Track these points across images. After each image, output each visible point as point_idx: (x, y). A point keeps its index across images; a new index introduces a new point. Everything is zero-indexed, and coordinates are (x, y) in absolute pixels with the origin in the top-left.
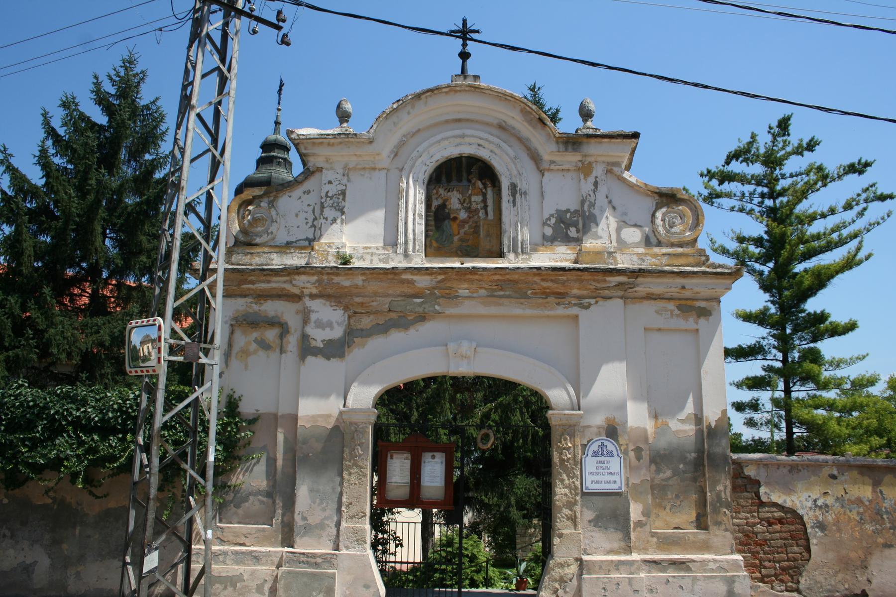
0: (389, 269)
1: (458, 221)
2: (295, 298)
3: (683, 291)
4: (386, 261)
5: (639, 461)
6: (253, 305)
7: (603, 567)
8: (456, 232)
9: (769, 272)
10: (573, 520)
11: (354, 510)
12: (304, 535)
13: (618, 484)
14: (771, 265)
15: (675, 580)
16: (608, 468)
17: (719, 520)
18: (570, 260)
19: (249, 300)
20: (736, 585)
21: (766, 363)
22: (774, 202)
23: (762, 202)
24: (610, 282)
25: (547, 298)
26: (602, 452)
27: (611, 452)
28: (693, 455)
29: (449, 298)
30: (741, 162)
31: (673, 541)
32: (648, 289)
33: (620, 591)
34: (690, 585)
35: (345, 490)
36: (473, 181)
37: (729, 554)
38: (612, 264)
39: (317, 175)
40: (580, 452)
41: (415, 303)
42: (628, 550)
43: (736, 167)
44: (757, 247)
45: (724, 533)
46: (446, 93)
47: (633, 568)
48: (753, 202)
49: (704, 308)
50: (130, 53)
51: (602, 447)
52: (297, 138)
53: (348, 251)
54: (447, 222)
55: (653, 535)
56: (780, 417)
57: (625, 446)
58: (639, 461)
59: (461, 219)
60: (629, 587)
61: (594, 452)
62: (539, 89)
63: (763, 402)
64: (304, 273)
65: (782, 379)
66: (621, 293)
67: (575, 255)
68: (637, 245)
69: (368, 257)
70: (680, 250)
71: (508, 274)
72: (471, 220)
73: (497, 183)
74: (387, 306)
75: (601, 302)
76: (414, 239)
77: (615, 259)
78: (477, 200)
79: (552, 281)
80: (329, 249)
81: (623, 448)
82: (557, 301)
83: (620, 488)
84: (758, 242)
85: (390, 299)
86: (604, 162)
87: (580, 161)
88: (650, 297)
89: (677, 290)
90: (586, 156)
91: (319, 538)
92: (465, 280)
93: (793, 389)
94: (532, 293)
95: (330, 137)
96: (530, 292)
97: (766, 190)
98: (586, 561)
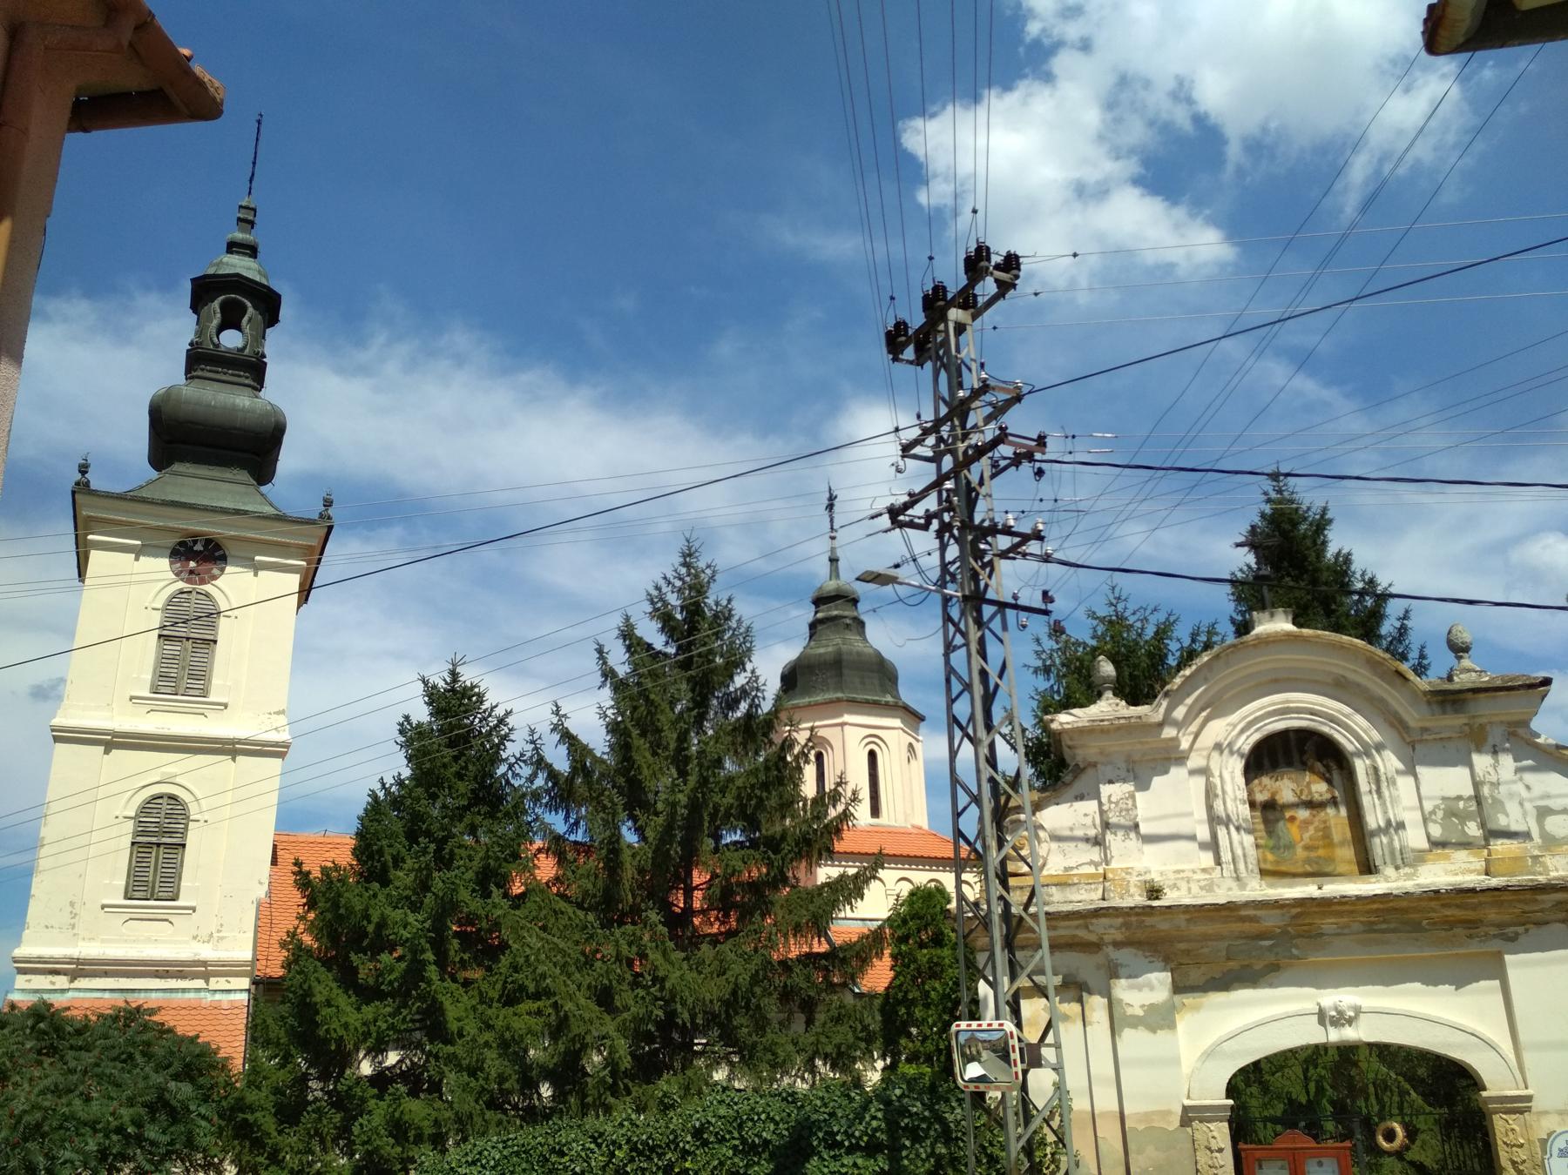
1: (1297, 823)
4: (1209, 888)
25: (1452, 929)
29: (1310, 937)
36: (1309, 764)
38: (1541, 874)
39: (1090, 772)
40: (1539, 1150)
41: (1261, 947)
50: (688, 541)
52: (1060, 727)
54: (1281, 824)
59: (1302, 818)
61: (1561, 1150)
64: (1105, 916)
67: (1484, 864)
69: (1183, 885)
74: (1224, 953)
75: (1533, 930)
76: (1245, 856)
78: (1319, 790)
79: (1458, 906)
80: (1128, 877)
85: (1226, 944)
86: (1502, 722)
87: (1465, 724)
90: (1474, 717)
94: (1428, 924)
96: (1425, 922)
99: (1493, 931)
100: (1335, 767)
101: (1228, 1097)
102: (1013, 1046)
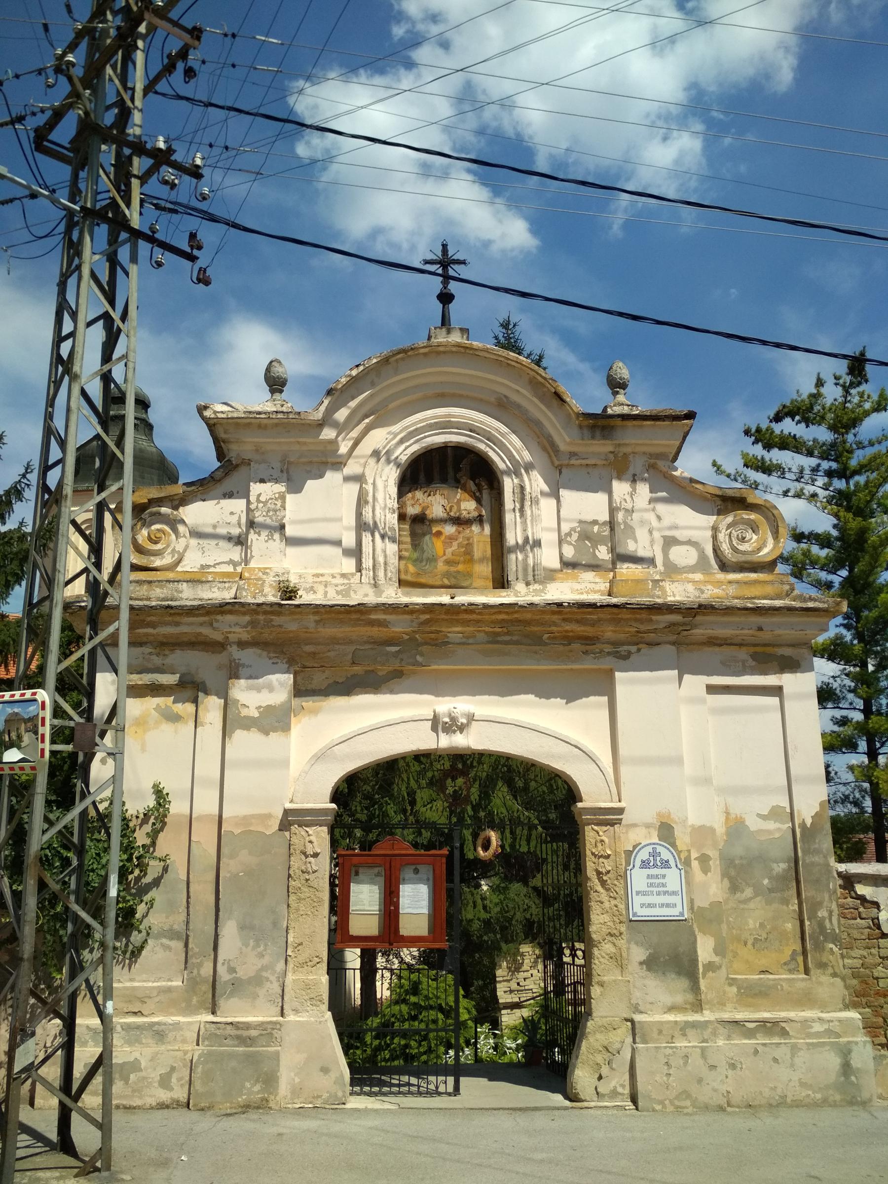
0: (353, 606)
1: (443, 538)
2: (217, 647)
3: (760, 633)
4: (346, 593)
5: (706, 874)
6: (154, 657)
7: (664, 1032)
8: (441, 553)
9: (841, 584)
10: (619, 961)
11: (303, 956)
12: (232, 995)
13: (679, 909)
14: (844, 573)
15: (767, 1049)
16: (664, 885)
17: (824, 960)
18: (599, 591)
19: (147, 650)
20: (854, 1055)
21: (838, 714)
22: (848, 483)
23: (830, 484)
24: (657, 622)
26: (652, 862)
27: (667, 861)
28: (783, 866)
29: (436, 645)
30: (799, 422)
31: (760, 992)
32: (711, 631)
33: (689, 1068)
34: (789, 1056)
35: (292, 924)
36: (462, 482)
37: (840, 1010)
38: (659, 597)
39: (243, 470)
42: (698, 1006)
43: (788, 426)
44: (822, 547)
45: (832, 980)
46: (425, 354)
47: (707, 1034)
48: (817, 483)
49: (790, 657)
51: (654, 854)
52: (213, 416)
53: (293, 580)
54: (427, 538)
55: (732, 982)
56: (862, 791)
57: (686, 854)
58: (706, 874)
60: (702, 1062)
61: (643, 862)
62: (514, 326)
63: (836, 769)
64: (230, 612)
65: (865, 738)
66: (673, 638)
68: (692, 569)
69: (320, 589)
70: (753, 576)
71: (516, 612)
72: (461, 535)
73: (496, 484)
74: (350, 656)
75: (645, 649)
76: (386, 564)
77: (663, 589)
79: (578, 621)
81: (683, 856)
82: (584, 648)
83: (682, 914)
84: (823, 541)
86: (644, 453)
87: (611, 452)
88: (713, 642)
89: (751, 632)
91: (254, 998)
92: (457, 621)
93: (881, 751)
94: (549, 638)
95: (263, 416)
96: (546, 636)
97: (834, 465)
98: (639, 1022)
99: (608, 648)
100: (486, 487)
101: (333, 800)
102: (43, 719)
